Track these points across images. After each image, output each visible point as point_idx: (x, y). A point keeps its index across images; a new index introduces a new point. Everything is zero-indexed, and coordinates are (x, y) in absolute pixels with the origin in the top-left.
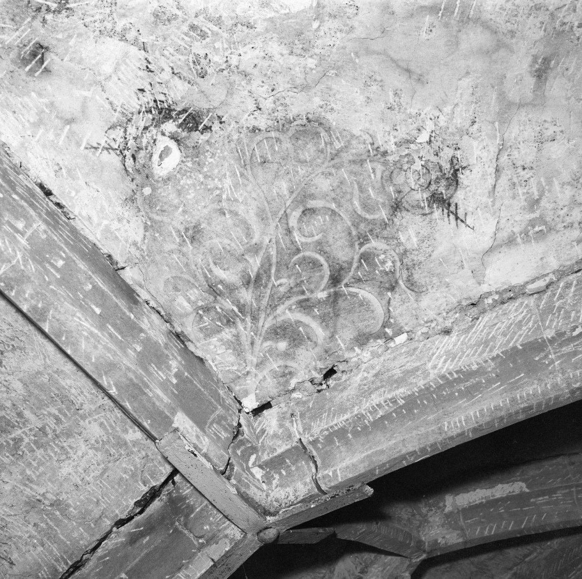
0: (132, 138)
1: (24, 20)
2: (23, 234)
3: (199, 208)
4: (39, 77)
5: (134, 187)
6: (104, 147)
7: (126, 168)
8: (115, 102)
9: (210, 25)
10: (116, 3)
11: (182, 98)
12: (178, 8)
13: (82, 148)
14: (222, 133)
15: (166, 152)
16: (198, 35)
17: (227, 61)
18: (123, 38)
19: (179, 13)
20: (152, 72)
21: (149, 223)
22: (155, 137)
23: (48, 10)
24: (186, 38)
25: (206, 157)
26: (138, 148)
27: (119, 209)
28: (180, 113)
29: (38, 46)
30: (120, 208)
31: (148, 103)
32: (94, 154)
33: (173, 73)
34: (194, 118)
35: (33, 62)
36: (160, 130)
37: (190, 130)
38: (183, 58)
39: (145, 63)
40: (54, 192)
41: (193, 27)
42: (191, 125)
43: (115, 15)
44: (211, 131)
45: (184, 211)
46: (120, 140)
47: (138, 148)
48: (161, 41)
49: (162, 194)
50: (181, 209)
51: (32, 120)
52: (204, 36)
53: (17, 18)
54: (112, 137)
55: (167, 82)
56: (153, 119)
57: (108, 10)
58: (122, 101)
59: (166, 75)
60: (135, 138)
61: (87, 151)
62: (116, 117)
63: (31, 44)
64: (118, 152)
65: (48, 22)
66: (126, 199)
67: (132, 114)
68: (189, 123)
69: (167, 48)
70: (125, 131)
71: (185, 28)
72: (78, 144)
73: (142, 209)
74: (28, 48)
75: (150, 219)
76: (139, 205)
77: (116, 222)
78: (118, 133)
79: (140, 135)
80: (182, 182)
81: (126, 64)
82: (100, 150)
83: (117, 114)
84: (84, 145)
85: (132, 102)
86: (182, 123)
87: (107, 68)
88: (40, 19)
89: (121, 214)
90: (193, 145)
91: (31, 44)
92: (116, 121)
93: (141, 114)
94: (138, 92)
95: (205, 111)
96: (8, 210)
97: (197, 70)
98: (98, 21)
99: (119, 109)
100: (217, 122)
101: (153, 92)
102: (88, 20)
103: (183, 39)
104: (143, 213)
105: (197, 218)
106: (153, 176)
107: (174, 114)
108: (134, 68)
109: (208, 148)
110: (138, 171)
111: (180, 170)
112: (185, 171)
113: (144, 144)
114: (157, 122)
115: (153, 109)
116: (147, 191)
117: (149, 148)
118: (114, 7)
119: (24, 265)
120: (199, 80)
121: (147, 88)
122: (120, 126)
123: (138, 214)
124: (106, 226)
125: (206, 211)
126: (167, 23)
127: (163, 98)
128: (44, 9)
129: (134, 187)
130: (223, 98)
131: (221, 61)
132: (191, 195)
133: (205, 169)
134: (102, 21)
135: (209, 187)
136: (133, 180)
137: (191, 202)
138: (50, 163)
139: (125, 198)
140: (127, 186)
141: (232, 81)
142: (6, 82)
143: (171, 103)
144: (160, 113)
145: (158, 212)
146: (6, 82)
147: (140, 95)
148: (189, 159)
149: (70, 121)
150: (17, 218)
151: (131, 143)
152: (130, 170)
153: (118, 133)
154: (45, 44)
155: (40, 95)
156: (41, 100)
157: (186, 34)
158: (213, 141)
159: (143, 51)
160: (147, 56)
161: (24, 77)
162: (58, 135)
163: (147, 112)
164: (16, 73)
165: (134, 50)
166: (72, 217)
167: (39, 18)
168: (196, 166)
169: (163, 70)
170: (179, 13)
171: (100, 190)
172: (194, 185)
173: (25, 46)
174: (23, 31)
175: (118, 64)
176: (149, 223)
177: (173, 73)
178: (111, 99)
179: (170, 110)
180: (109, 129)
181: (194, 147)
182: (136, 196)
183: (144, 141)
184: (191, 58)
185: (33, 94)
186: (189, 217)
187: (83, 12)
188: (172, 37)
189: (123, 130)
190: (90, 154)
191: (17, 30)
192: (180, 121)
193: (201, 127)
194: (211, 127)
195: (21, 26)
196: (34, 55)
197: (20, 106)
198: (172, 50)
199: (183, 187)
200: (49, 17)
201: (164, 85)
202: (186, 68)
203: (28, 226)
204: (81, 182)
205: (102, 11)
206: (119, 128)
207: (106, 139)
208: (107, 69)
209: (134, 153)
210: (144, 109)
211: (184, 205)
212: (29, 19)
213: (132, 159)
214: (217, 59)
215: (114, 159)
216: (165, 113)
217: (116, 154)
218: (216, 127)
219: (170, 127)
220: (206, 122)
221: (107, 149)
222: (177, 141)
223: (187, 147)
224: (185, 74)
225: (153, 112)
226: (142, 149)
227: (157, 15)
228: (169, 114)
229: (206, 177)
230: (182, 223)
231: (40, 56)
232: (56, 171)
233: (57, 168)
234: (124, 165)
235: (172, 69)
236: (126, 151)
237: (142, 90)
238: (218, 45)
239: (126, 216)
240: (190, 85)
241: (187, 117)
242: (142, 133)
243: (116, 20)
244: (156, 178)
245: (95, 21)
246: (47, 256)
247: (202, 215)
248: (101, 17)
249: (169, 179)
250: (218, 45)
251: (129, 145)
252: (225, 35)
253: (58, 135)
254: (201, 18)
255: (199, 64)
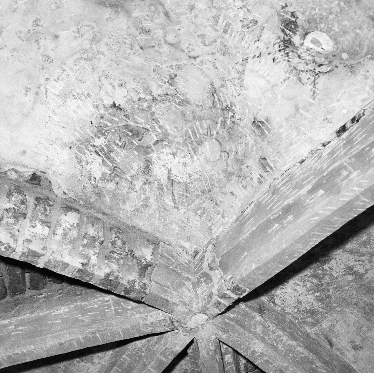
0: (306, 67)
1: (240, 131)
2: (350, 173)
3: (356, 17)
4: (271, 125)
5: (342, 66)
6: (314, 87)
7: (328, 72)
8: (283, 77)
9: (220, 21)
10: (223, 78)
11: (274, 33)
12: (216, 42)
13: (313, 102)
14: (294, 5)
15: (315, 42)
16: (229, 28)
17: (241, 8)
18: (242, 73)
19: (219, 41)
20: (260, 54)
21: (369, 56)
22: (305, 50)
23: (233, 117)
24: (233, 34)
25: (315, 14)
26: (313, 62)
27: (359, 78)
28: (285, 34)
29: (254, 124)
30: (358, 77)
31: (282, 55)
32: (318, 94)
33: (258, 40)
34: (288, 24)
35: (263, 128)
36: (299, 46)
37: (296, 26)
38: (247, 35)
39: (256, 58)
40: (343, 124)
41: (225, 32)
42: (292, 26)
43: (230, 78)
44: (294, 12)
45: (360, 29)
46: (308, 75)
47: (313, 62)
48: (239, 50)
49: (347, 44)
50: (358, 31)
51: (295, 134)
52: (228, 25)
53: (240, 135)
54: (306, 81)
55: (265, 44)
56: (292, 51)
57: (228, 82)
58: (282, 73)
59: (261, 45)
60: (307, 64)
61: (316, 99)
62: (293, 78)
63: (253, 128)
64: (317, 77)
65: (240, 117)
66: (351, 72)
67: (290, 66)
68: (291, 27)
69: (243, 46)
70: (302, 71)
71: (227, 36)
72: (311, 104)
73: (359, 61)
74: (255, 130)
75: (366, 55)
76: (356, 63)
77: (368, 81)
78: (303, 76)
79: (304, 61)
80: (337, 30)
81: (259, 70)
82: (316, 90)
83: (291, 77)
84: (311, 100)
85: (282, 66)
86: (293, 32)
87: (262, 82)
88: (238, 122)
89: (362, 77)
90: (307, 23)
91: (253, 128)
92: (296, 77)
93: (290, 60)
94: (275, 62)
95: (280, 18)
96: (334, 179)
97: (253, 26)
98: (235, 88)
99: (288, 75)
100: (287, 9)
101: (274, 53)
102: (235, 94)
103: (234, 37)
104: (362, 60)
105: (365, 19)
106: (334, 52)
107: (287, 38)
108: (259, 66)
109: (308, 13)
110: (330, 62)
111: (328, 31)
112: (328, 28)
113: (311, 58)
114: (294, 49)
115: (286, 52)
116: (345, 56)
117: (313, 54)
118: (225, 79)
119: (362, 188)
120: (259, 24)
121: (272, 56)
122: (299, 75)
123: (362, 64)
124: (370, 88)
125: (359, 12)
126: (227, 47)
127: (277, 46)
128: (232, 119)
129: (342, 66)
130: (268, 7)
131: (242, 12)
132: (346, 23)
133: (325, 14)
134: (235, 85)
135: (339, 10)
136: (337, 67)
137: (352, 24)
138: (323, 125)
139: (350, 73)
140: (341, 71)
141: (254, 3)
142: (274, 147)
143: (279, 40)
144: (288, 47)
145: (361, 48)
146: (274, 147)
147: (277, 61)
148: (318, 26)
149: (297, 108)
150: (340, 174)
151: (310, 67)
152: (329, 69)
153: (303, 76)
154: (253, 120)
155: (281, 127)
156: (284, 126)
157: (231, 35)
158: (302, 10)
159: (248, 61)
160: (251, 58)
161: (271, 135)
162: (305, 118)
163: (288, 56)
164: (269, 139)
165: (249, 66)
166: (362, 111)
167: (238, 122)
168: (323, 21)
169: (258, 47)
170: (219, 41)
171: (343, 92)
172: (338, 21)
173: (254, 132)
174: (246, 132)
175: (259, 76)
176: (369, 56)
177: (258, 40)
178: (281, 80)
179: (284, 41)
180: (301, 82)
181: (309, 23)
182: (349, 65)
183: (308, 58)
184: (245, 30)
185: (280, 131)
186: (364, 25)
187: (231, 97)
188: (235, 43)
189: (301, 73)
190: (318, 97)
191: (246, 136)
192: (291, 33)
193: (293, 19)
194: (291, 12)
195: (244, 133)
196: (259, 127)
197: (287, 140)
198: (243, 43)
199: (341, 29)
200: (237, 117)
201: (268, 46)
202: (254, 33)
203: (345, 168)
204: (336, 104)
205: (229, 85)
206: (300, 76)
207: (308, 84)
208: (262, 82)
209: (317, 65)
210: (286, 58)
211: (355, 28)
212: (239, 128)
213: (322, 67)
214: (241, 14)
215: (322, 80)
216: (287, 44)
217: (318, 78)
218: (291, 9)
219: (296, 39)
220: (289, 17)
221: (315, 84)
222: (306, 34)
223: (310, 27)
224: (258, 33)
225: (288, 51)
226: (314, 59)
227: (224, 53)
228: (287, 41)
229: (331, 13)
230: (370, 30)
231: (259, 124)
232: (328, 122)
233: (326, 121)
234: (326, 73)
235: (256, 41)
236: (316, 71)
237: (274, 60)
238: (232, 15)
239: (364, 73)
240: (264, 29)
241: (287, 29)
242: (303, 59)
243: (232, 77)
244: (335, 49)
245: (236, 90)
246: (368, 159)
247: (362, 14)
248: (232, 86)
249: (335, 40)
250: (232, 15)
251: (311, 69)
252: (224, 12)
253: (305, 118)
254: (217, 28)
255: (248, 25)
